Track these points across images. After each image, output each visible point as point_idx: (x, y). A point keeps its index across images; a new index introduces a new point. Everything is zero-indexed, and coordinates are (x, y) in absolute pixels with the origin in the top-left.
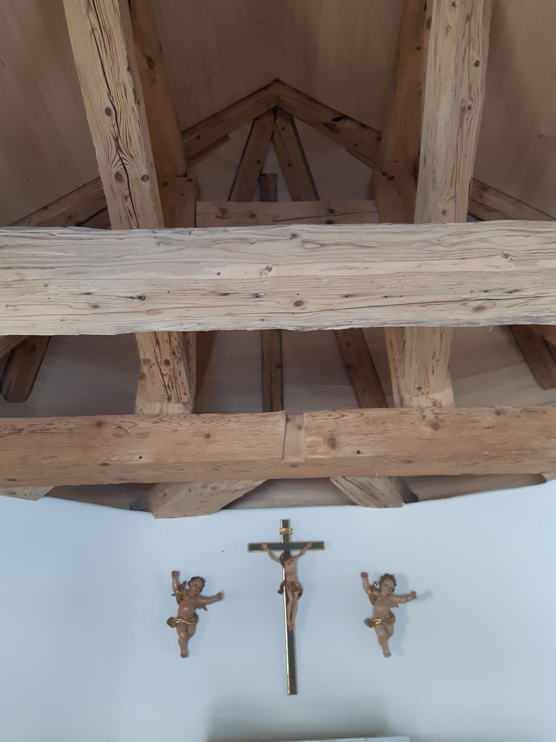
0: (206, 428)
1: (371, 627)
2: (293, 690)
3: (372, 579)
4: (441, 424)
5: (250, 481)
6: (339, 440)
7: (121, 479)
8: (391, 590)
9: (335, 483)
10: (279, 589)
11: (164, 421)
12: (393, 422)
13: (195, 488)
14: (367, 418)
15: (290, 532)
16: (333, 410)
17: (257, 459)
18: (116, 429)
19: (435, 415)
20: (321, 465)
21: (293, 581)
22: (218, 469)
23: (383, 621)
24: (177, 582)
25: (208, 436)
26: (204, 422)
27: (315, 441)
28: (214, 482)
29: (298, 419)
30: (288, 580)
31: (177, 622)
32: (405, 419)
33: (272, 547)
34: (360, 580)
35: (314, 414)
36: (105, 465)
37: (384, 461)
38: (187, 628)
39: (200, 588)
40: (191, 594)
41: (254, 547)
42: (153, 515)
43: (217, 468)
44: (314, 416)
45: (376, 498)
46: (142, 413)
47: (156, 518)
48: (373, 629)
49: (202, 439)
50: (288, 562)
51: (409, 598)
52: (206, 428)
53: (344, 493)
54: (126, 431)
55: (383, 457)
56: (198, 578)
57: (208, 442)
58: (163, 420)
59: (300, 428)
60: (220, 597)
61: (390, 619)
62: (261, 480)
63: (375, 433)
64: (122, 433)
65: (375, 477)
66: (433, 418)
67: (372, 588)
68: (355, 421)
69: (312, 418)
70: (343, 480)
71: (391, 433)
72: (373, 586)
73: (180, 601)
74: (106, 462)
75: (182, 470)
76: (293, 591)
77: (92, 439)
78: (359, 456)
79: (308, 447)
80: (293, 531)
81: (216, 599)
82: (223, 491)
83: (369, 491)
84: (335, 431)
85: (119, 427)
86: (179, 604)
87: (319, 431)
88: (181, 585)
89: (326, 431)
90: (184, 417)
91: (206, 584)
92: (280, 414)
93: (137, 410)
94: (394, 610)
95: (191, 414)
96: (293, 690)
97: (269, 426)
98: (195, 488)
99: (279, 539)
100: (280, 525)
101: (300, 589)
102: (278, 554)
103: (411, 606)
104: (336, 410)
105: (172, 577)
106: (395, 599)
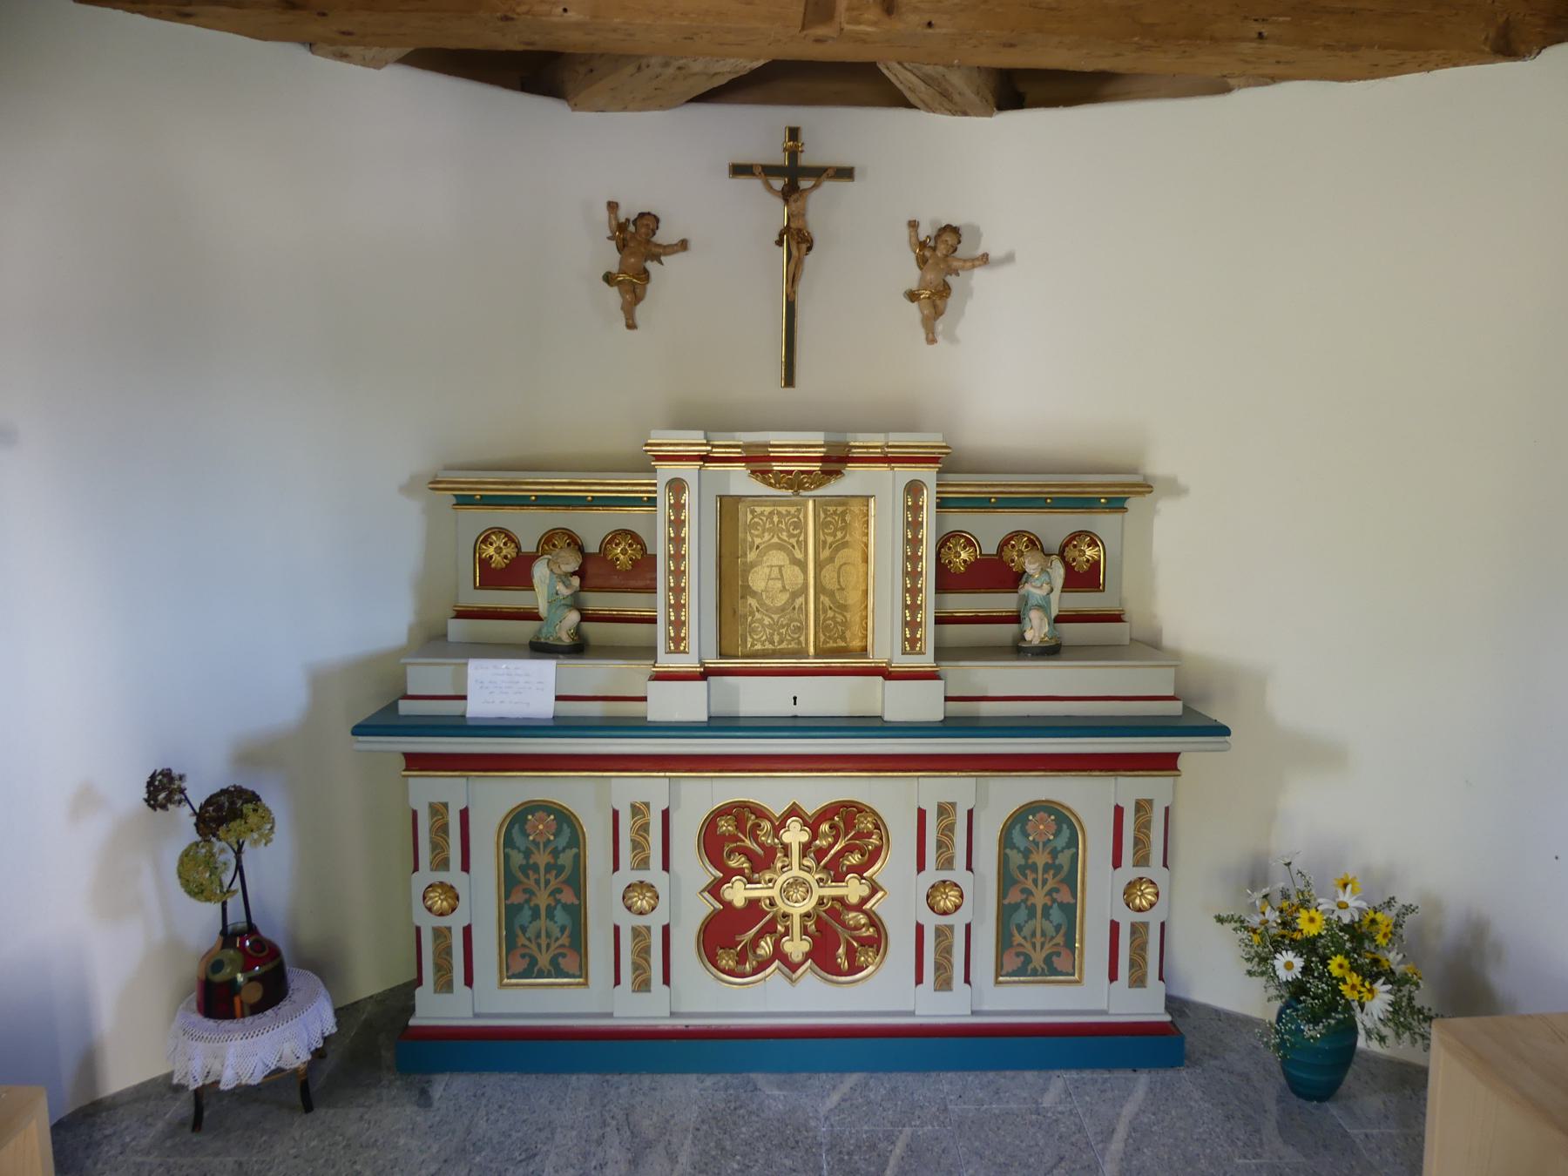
1: (913, 301)
2: (789, 380)
3: (925, 231)
5: (741, 60)
7: (528, 44)
8: (951, 250)
9: (885, 72)
10: (777, 238)
13: (648, 66)
20: (864, 42)
23: (933, 294)
24: (616, 218)
30: (792, 225)
33: (769, 171)
38: (634, 289)
42: (569, 105)
45: (951, 101)
47: (573, 110)
50: (794, 196)
51: (977, 263)
56: (649, 214)
60: (683, 245)
61: (944, 291)
65: (953, 66)
67: (923, 245)
70: (899, 67)
72: (925, 241)
74: (510, 14)
76: (798, 243)
78: (930, 31)
80: (804, 148)
88: (622, 223)
94: (951, 280)
96: (789, 380)
99: (781, 159)
102: (778, 184)
103: (979, 276)
105: (608, 210)
106: (956, 264)
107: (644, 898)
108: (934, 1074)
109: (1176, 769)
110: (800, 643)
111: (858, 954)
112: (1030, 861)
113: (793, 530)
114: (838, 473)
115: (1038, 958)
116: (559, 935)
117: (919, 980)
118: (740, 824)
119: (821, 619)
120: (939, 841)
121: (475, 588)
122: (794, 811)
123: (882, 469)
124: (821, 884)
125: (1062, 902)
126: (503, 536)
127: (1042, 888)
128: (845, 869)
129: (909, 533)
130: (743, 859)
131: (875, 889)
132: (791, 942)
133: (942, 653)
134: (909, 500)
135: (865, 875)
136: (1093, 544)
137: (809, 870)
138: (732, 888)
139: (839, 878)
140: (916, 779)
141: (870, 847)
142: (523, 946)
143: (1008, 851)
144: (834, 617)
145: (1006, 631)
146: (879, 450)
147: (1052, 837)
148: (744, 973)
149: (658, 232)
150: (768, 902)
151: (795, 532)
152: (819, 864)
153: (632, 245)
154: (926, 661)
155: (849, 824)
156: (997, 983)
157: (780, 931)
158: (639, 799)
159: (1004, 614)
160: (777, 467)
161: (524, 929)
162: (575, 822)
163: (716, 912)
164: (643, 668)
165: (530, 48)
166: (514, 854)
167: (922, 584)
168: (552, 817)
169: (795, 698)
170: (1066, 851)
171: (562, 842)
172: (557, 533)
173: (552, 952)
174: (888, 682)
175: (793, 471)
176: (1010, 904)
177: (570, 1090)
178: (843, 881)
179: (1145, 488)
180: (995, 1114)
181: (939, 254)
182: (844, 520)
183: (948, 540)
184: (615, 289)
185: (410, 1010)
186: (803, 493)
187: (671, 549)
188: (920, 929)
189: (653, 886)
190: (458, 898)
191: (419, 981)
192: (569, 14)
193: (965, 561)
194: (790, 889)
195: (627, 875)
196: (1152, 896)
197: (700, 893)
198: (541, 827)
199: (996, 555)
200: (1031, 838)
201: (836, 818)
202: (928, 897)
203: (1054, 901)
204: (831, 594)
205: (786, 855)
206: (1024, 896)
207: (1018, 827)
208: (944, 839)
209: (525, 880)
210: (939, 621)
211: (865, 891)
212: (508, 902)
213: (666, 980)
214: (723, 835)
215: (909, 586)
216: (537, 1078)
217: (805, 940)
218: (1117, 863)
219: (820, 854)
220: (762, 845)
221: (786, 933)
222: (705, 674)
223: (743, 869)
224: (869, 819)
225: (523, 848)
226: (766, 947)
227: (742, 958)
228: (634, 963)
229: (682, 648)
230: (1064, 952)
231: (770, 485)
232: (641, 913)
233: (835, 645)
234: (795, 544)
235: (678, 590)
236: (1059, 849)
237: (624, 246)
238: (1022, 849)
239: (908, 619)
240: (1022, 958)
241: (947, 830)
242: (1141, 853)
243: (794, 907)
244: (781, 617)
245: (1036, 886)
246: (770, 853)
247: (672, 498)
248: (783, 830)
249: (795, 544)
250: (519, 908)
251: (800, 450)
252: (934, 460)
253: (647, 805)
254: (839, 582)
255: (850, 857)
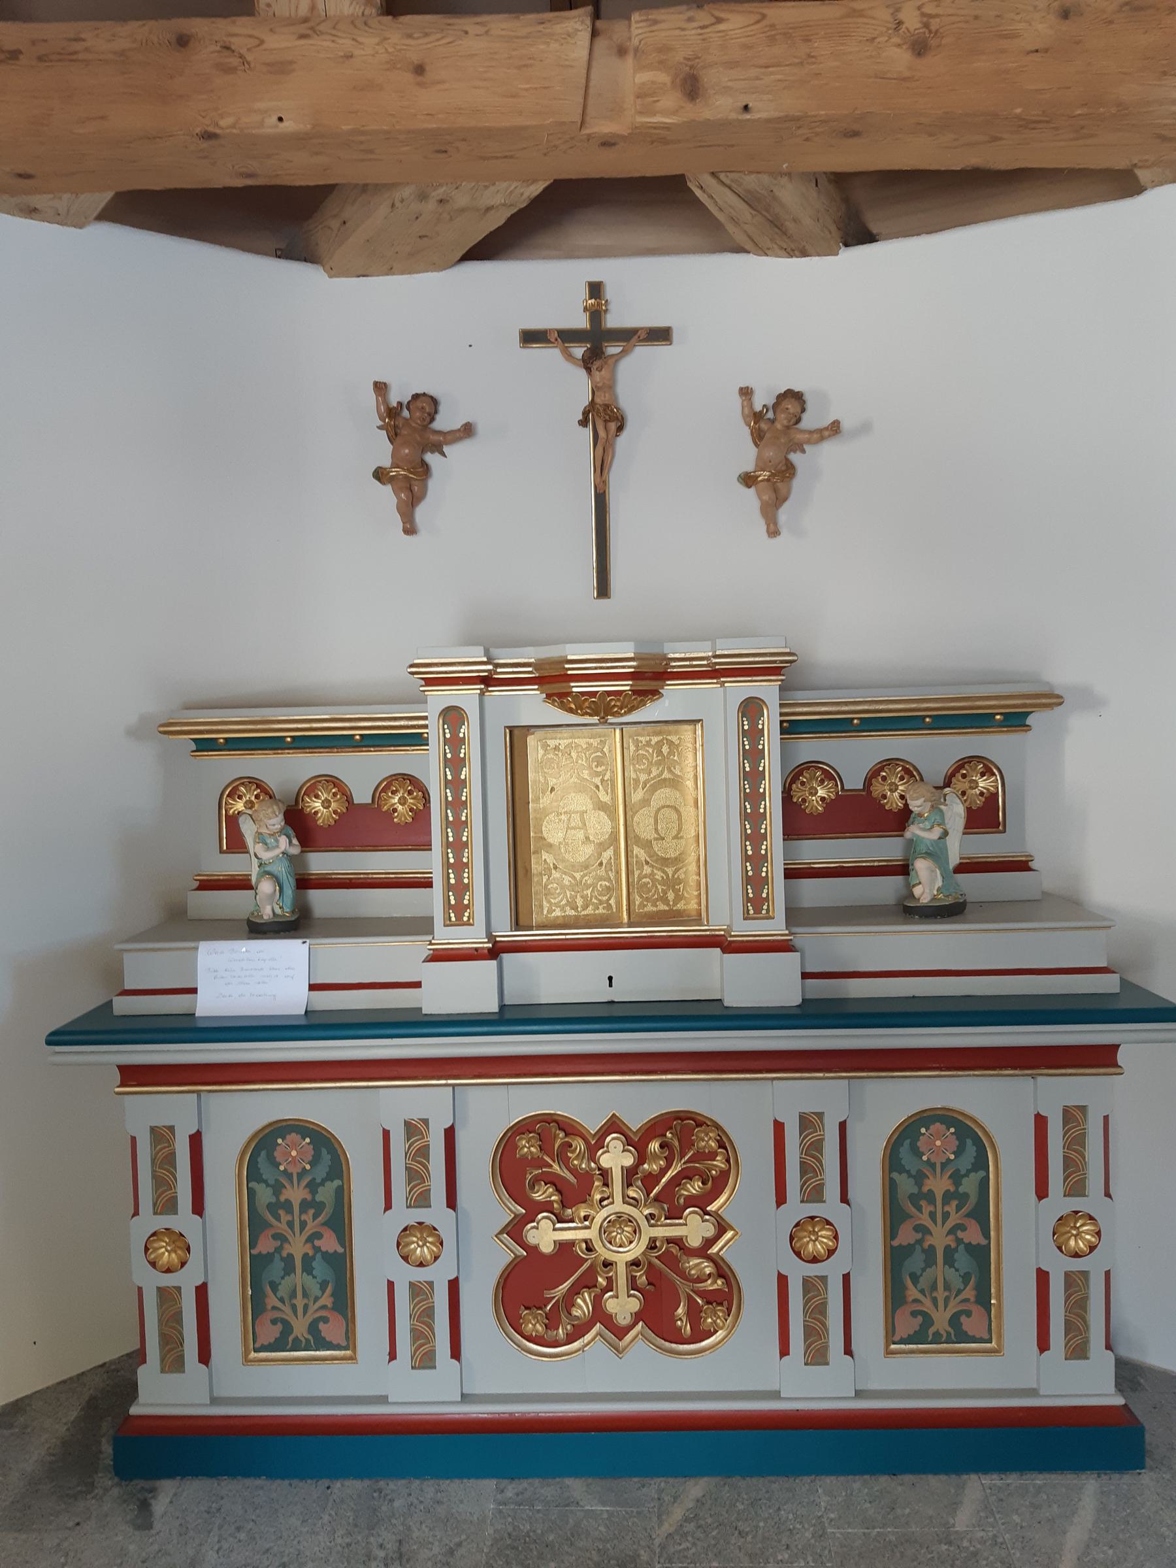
0: (415, 50)
1: (749, 487)
2: (603, 590)
4: (933, 43)
6: (705, 80)
8: (794, 420)
9: (698, 193)
10: (580, 417)
11: (322, 33)
12: (830, 37)
14: (773, 26)
15: (604, 308)
16: (698, 7)
17: (528, 123)
18: (218, 52)
19: (925, 19)
20: (664, 141)
21: (607, 402)
22: (446, 152)
23: (773, 475)
24: (386, 402)
25: (419, 70)
26: (410, 36)
27: (653, 82)
28: (441, 185)
29: (617, 30)
30: (598, 400)
31: (391, 474)
32: (856, 30)
33: (567, 337)
34: (737, 401)
35: (655, 14)
36: (208, 136)
37: (800, 132)
39: (429, 414)
40: (414, 425)
41: (531, 337)
43: (443, 149)
44: (655, 22)
46: (271, 14)
47: (330, 277)
48: (752, 490)
49: (409, 77)
50: (597, 364)
52: (415, 50)
53: (716, 219)
54: (241, 56)
55: (798, 119)
56: (424, 394)
57: (421, 85)
58: (320, 31)
59: (622, 52)
60: (468, 430)
61: (787, 471)
62: (540, 183)
63: (787, 63)
64: (234, 61)
66: (919, 25)
67: (758, 416)
68: (747, 34)
69: (650, 26)
71: (821, 63)
72: (761, 412)
73: (394, 436)
74: (211, 129)
75: (371, 152)
76: (606, 421)
77: (172, 77)
78: (748, 116)
79: (638, 97)
80: (611, 307)
81: (462, 435)
82: (463, 210)
83: (767, 211)
84: (699, 58)
85: (228, 48)
86: (392, 442)
87: (665, 57)
89: (679, 56)
90: (366, 24)
91: (442, 408)
92: (579, 16)
93: (259, 7)
94: (795, 457)
95: (379, 15)
96: (603, 590)
97: (554, 46)
98: (402, 201)
99: (581, 322)
100: (584, 292)
101: (620, 418)
102: (579, 351)
103: (828, 451)
104: (705, 7)
106: (800, 437)
107: (424, 1244)
108: (807, 1479)
109: (1116, 1065)
110: (609, 907)
111: (703, 1314)
112: (925, 1189)
113: (597, 766)
114: (655, 693)
115: (941, 1320)
116: (319, 1293)
117: (784, 1351)
118: (545, 1145)
119: (636, 876)
120: (803, 1164)
121: (221, 851)
122: (613, 1125)
123: (708, 687)
124: (652, 1222)
125: (970, 1243)
126: (254, 787)
127: (943, 1224)
128: (682, 1201)
129: (747, 765)
130: (551, 1190)
131: (722, 1229)
132: (615, 1300)
133: (794, 915)
134: (746, 723)
135: (708, 1208)
136: (987, 772)
137: (635, 1203)
138: (537, 1228)
139: (675, 1214)
140: (770, 1082)
141: (714, 1172)
142: (274, 1308)
143: (895, 1175)
144: (652, 874)
145: (886, 889)
146: (705, 662)
147: (952, 1157)
148: (556, 1340)
149: (438, 417)
150: (584, 1245)
151: (599, 769)
152: (648, 1195)
153: (406, 433)
154: (774, 927)
155: (686, 1142)
156: (889, 1353)
157: (601, 1284)
158: (415, 1115)
159: (876, 864)
160: (577, 688)
161: (274, 1287)
162: (337, 1146)
163: (518, 1260)
164: (419, 947)
165: (249, 182)
166: (260, 1188)
167: (766, 829)
168: (308, 1140)
169: (610, 978)
170: (972, 1174)
171: (321, 1172)
172: (320, 782)
173: (310, 1317)
174: (726, 955)
175: (598, 692)
176: (900, 1245)
177: (330, 1504)
178: (681, 1218)
179: (1051, 700)
180: (890, 1542)
181: (778, 426)
182: (660, 753)
183: (800, 773)
184: (389, 488)
185: (130, 1391)
186: (611, 719)
187: (449, 794)
188: (782, 1280)
189: (435, 1229)
190: (188, 1250)
191: (140, 1356)
192: (285, 124)
193: (823, 799)
194: (612, 1229)
195: (403, 1215)
196: (1093, 1236)
197: (496, 1236)
198: (294, 1153)
199: (863, 790)
200: (925, 1158)
201: (669, 1135)
202: (792, 1238)
203: (959, 1241)
204: (647, 845)
205: (606, 1184)
206: (919, 1236)
207: (908, 1142)
208: (810, 1161)
209: (279, 1225)
210: (790, 874)
211: (709, 1230)
212: (254, 1252)
213: (456, 1353)
214: (524, 1157)
215: (749, 831)
216: (291, 1485)
217: (634, 1296)
218: (1042, 1192)
219: (650, 1180)
220: (574, 1171)
221: (609, 1288)
222: (496, 951)
223: (551, 1202)
224: (711, 1135)
225: (271, 1182)
226: (583, 1305)
227: (552, 1322)
228: (413, 1330)
229: (465, 919)
230: (977, 1310)
231: (571, 711)
232: (421, 1265)
233: (655, 909)
234: (599, 784)
235: (459, 846)
236: (963, 1172)
237: (396, 434)
238: (913, 1173)
239: (750, 873)
240: (920, 1319)
241: (813, 1149)
242: (1074, 1178)
243: (619, 1252)
244: (585, 875)
245: (935, 1222)
246: (585, 1180)
247: (447, 731)
248: (600, 1152)
249: (599, 784)
250: (267, 1259)
251: (604, 665)
252: (776, 671)
253: (426, 1122)
254: (656, 830)
255: (688, 1186)
